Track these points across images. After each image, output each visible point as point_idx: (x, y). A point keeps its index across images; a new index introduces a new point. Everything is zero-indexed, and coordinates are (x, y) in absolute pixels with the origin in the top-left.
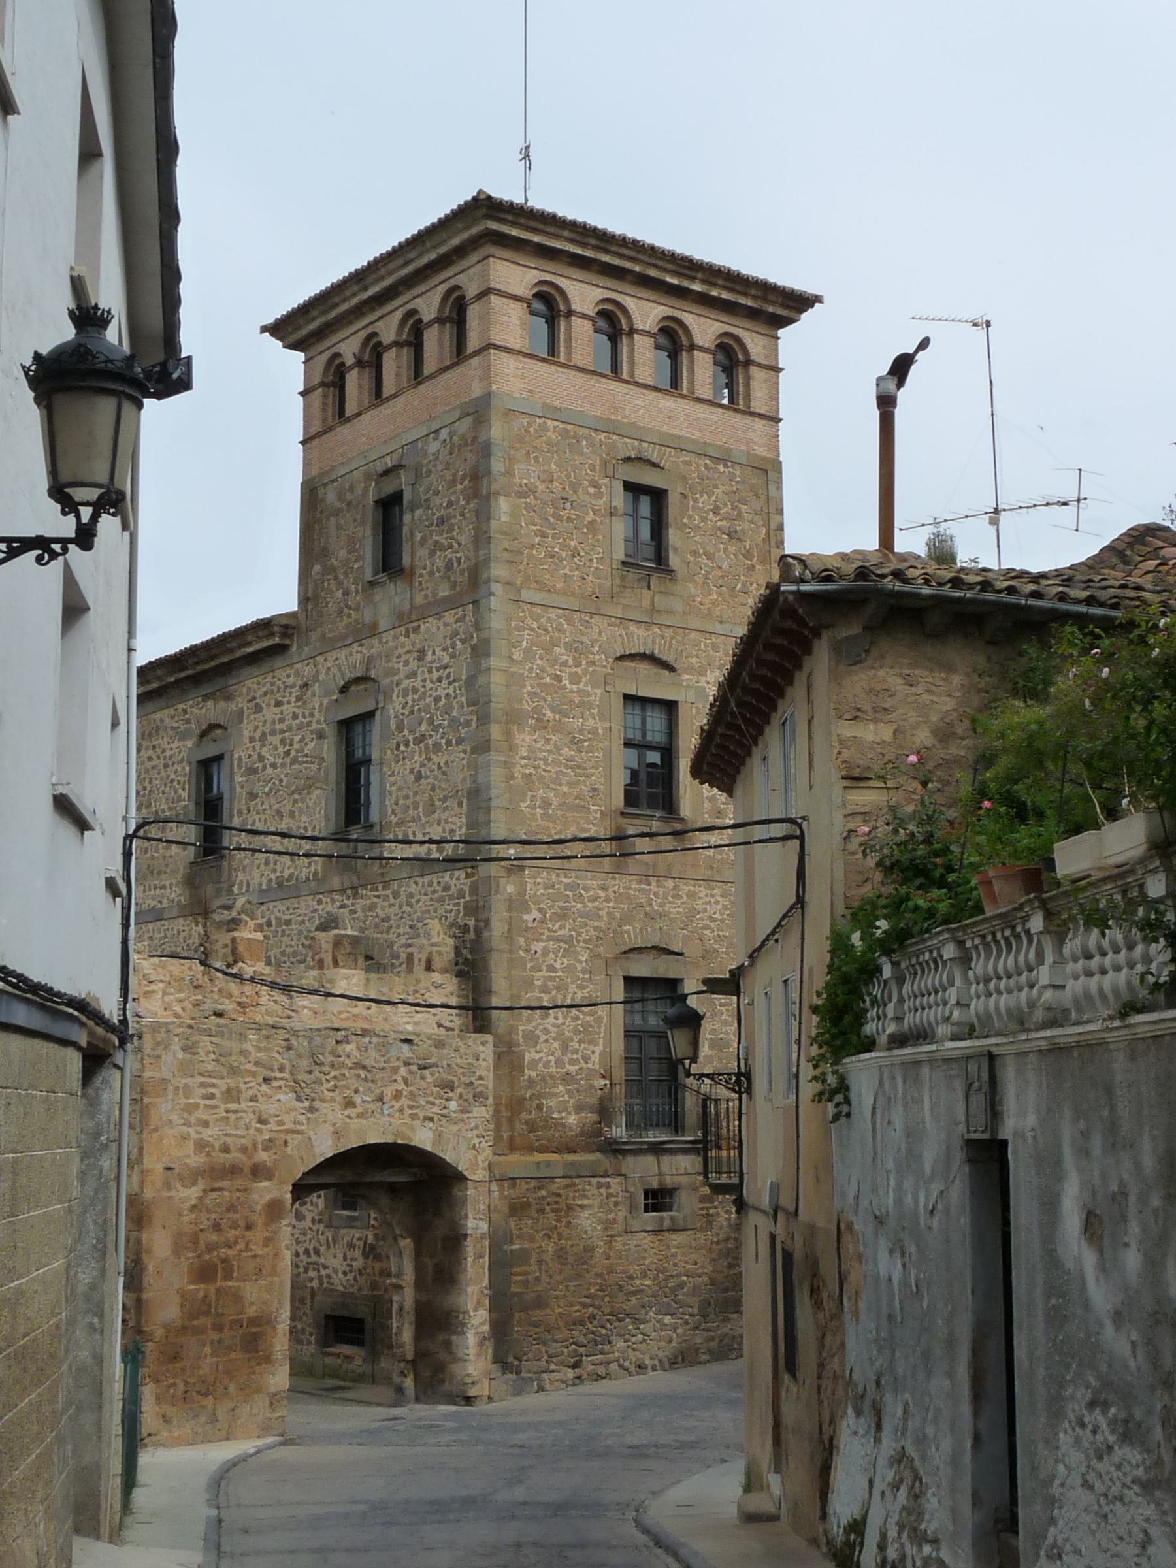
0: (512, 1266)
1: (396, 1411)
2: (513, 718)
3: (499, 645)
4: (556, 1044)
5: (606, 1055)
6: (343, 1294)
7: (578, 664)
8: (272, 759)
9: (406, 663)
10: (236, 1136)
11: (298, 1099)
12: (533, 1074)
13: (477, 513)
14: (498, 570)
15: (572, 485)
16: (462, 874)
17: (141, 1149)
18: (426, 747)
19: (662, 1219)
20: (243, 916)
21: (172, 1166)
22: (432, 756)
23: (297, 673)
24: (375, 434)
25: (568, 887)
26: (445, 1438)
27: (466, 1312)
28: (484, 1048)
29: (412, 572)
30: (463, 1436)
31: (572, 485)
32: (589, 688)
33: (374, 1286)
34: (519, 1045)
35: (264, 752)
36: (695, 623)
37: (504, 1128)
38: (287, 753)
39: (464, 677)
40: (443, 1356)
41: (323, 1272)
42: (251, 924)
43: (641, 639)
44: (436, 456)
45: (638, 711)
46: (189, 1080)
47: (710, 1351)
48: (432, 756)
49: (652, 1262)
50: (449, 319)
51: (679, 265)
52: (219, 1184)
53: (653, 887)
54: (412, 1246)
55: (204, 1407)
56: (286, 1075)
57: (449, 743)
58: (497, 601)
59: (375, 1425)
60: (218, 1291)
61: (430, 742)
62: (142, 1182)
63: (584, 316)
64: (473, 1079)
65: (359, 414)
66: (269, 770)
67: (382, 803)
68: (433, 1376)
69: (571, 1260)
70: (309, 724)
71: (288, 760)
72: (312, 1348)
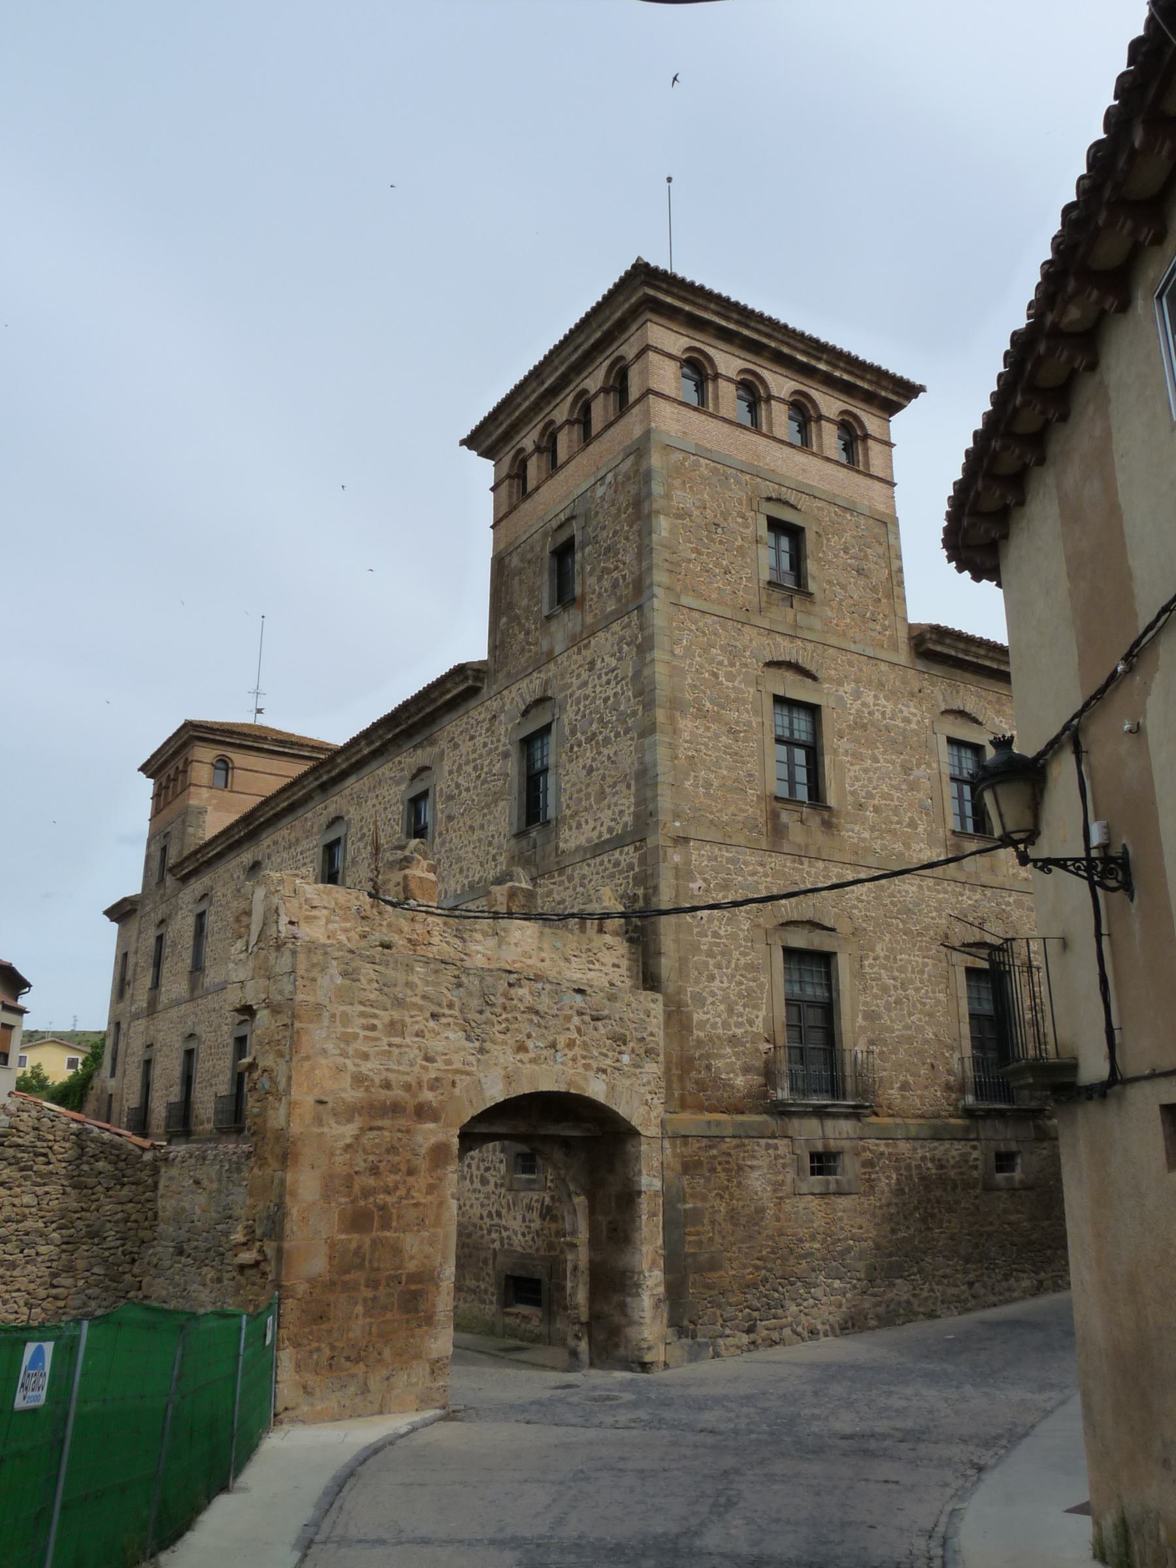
0: (685, 1226)
1: (571, 1377)
2: (676, 705)
3: (661, 640)
4: (722, 1007)
5: (770, 1021)
6: (523, 1256)
7: (732, 665)
8: (466, 785)
9: (579, 676)
10: (398, 1072)
11: (468, 1038)
12: (701, 1034)
13: (640, 532)
14: (659, 577)
15: (722, 513)
16: (631, 848)
17: (290, 1078)
18: (597, 743)
19: (828, 1182)
20: (416, 855)
21: (325, 1099)
22: (602, 749)
23: (487, 709)
24: (552, 498)
25: (729, 860)
26: (623, 1417)
27: (642, 1272)
28: (654, 1005)
29: (583, 596)
30: (642, 1414)
31: (722, 513)
32: (743, 686)
33: (551, 1246)
34: (688, 1006)
35: (461, 780)
36: (832, 640)
37: (675, 1086)
38: (479, 777)
39: (630, 675)
40: (618, 1319)
41: (504, 1234)
42: (424, 864)
43: (787, 650)
44: (603, 498)
45: (786, 712)
46: (347, 1008)
47: (878, 1317)
48: (602, 749)
49: (820, 1226)
50: (613, 388)
51: (806, 345)
52: (379, 1123)
53: (806, 866)
54: (586, 1203)
55: (353, 1376)
56: (456, 1013)
57: (617, 735)
58: (660, 604)
59: (548, 1394)
60: (374, 1241)
61: (601, 738)
62: (289, 1115)
63: (729, 380)
64: (645, 1035)
65: (537, 488)
66: (464, 794)
67: (558, 800)
68: (608, 1342)
69: (743, 1221)
70: (496, 748)
71: (479, 783)
72: (494, 1308)
